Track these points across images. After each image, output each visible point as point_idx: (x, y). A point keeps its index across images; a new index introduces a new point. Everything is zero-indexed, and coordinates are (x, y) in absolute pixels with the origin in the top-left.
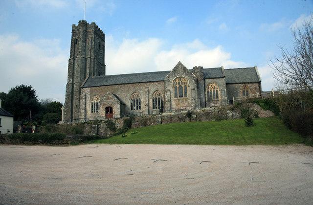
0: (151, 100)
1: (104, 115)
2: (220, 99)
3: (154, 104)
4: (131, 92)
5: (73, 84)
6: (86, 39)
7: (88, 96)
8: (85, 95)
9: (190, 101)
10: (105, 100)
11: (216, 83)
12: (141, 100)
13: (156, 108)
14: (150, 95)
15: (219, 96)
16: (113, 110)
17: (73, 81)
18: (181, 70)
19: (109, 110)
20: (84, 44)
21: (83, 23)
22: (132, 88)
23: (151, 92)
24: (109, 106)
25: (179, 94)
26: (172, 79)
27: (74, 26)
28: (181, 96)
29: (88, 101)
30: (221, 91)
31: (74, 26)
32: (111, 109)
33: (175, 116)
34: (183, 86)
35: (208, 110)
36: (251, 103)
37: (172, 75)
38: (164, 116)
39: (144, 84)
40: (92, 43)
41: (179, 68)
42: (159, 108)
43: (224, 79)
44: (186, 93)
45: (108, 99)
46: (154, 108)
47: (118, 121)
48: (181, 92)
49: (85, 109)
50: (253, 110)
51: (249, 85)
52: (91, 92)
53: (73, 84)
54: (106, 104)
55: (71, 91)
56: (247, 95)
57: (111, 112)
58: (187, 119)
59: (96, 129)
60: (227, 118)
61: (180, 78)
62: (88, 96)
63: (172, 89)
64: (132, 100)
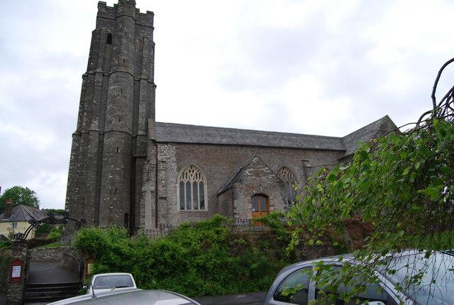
24: (261, 191)
45: (258, 175)
54: (253, 188)
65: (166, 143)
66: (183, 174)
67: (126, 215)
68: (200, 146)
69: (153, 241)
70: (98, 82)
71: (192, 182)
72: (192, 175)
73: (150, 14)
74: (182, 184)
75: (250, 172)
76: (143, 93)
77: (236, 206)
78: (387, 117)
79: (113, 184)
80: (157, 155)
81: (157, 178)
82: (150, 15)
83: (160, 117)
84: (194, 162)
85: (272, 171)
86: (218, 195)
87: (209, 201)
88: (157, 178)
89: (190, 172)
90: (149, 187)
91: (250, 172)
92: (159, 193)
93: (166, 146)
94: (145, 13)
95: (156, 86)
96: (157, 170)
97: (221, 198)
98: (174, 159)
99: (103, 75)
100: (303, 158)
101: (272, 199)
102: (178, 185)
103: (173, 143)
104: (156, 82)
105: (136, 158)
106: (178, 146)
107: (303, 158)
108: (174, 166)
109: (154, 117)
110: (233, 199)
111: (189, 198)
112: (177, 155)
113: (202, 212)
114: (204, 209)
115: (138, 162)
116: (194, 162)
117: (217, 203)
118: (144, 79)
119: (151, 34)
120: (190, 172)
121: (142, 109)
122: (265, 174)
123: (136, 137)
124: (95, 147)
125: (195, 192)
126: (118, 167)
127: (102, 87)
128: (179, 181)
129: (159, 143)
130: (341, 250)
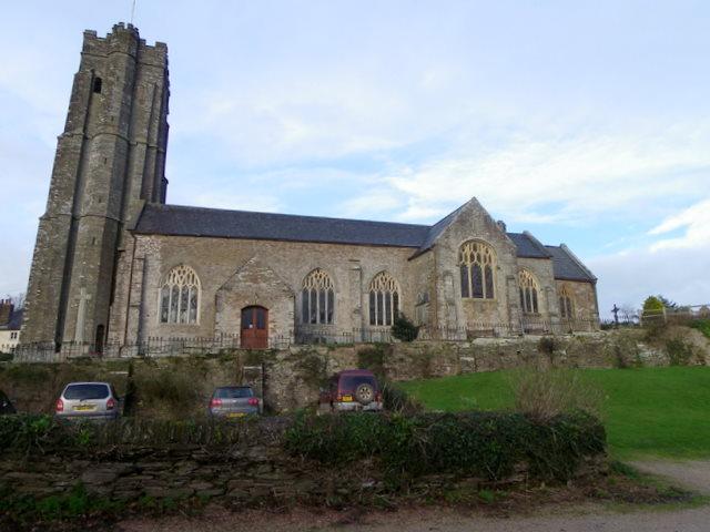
0: (367, 298)
1: (237, 332)
2: (541, 310)
3: (372, 310)
4: (307, 269)
5: (74, 219)
6: (134, 85)
7: (155, 264)
8: (145, 260)
9: (503, 311)
10: (242, 284)
11: (533, 270)
12: (337, 297)
13: (380, 323)
14: (364, 282)
15: (540, 303)
16: (270, 318)
17: (74, 209)
18: (478, 224)
19: (254, 316)
20: (129, 98)
21: (128, 36)
22: (309, 255)
23: (368, 276)
24: (258, 302)
25: (473, 286)
26: (456, 244)
27: (90, 36)
28: (478, 294)
29: (153, 281)
30: (546, 290)
31: (90, 36)
32: (262, 310)
33: (508, 348)
34: (483, 266)
35: (591, 337)
36: (686, 328)
37: (456, 231)
38: (480, 348)
39: (347, 248)
40: (154, 101)
41: (470, 217)
42: (388, 323)
43: (549, 262)
44: (490, 286)
45: (255, 280)
46: (372, 322)
47: (337, 353)
48: (477, 282)
49: (141, 308)
50: (691, 346)
51: (573, 284)
52: (166, 253)
53: (74, 219)
54: (246, 297)
55: (66, 240)
56: (570, 316)
57: (262, 325)
58: (544, 360)
59: (258, 383)
60: (640, 363)
61: (475, 244)
62: (155, 264)
63: (456, 271)
64: (166, 287)
71: (180, 286)
73: (162, 47)
75: (243, 277)
77: (217, 320)
78: (474, 199)
82: (162, 47)
85: (276, 274)
87: (202, 313)
89: (179, 272)
90: (117, 290)
91: (243, 277)
92: (132, 301)
94: (154, 45)
95: (41, 219)
100: (350, 256)
107: (350, 256)
112: (163, 250)
122: (266, 280)
126: (93, 264)
130: (29, 472)
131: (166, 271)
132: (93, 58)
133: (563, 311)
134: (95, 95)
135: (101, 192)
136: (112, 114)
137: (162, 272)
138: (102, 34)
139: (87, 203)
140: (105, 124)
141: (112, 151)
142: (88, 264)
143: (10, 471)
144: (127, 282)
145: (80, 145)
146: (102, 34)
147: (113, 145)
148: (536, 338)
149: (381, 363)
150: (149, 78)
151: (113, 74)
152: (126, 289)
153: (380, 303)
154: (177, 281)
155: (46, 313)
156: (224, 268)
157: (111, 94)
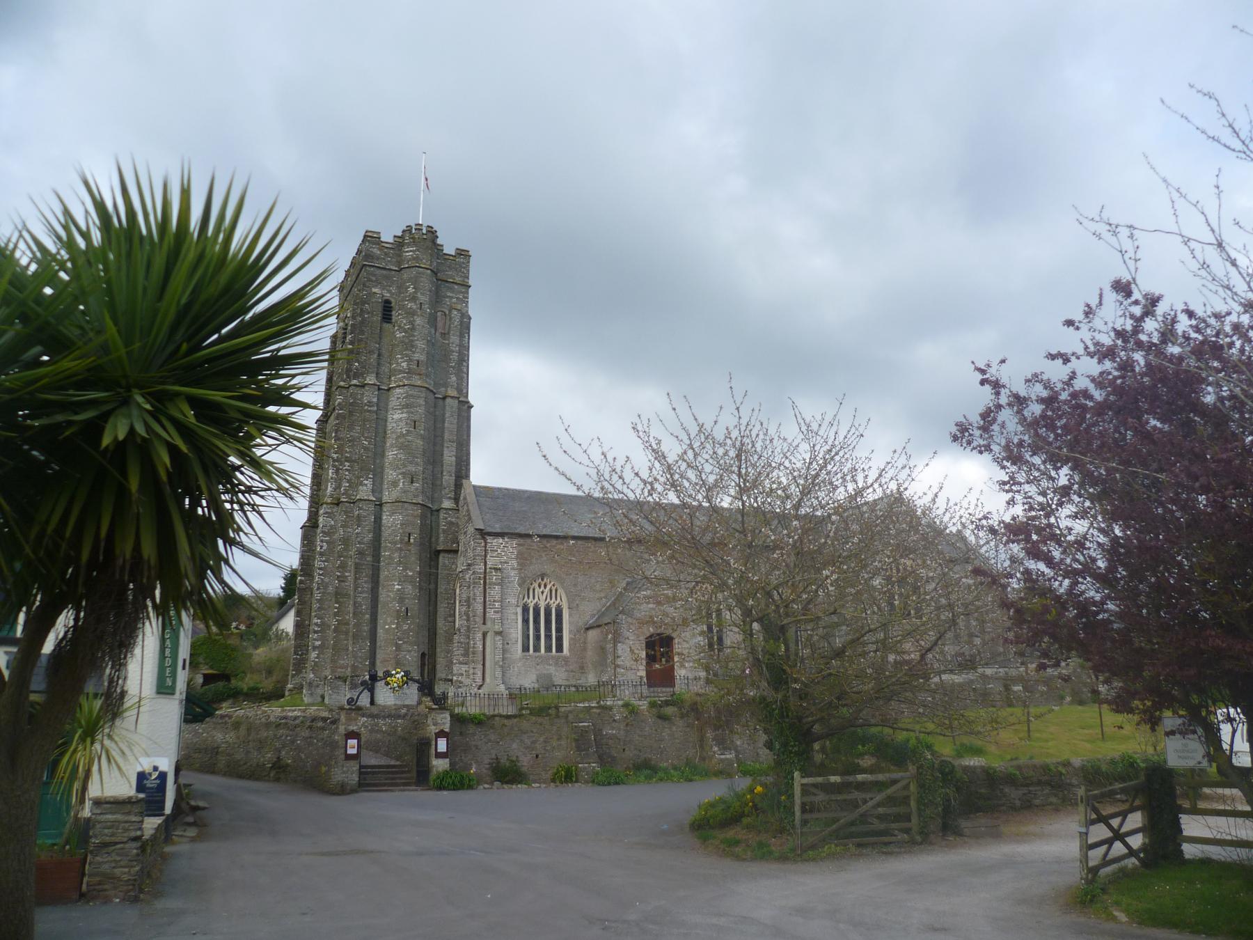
31: (370, 238)
65: (501, 535)
66: (551, 591)
67: (423, 655)
68: (560, 541)
69: (440, 769)
70: (370, 404)
72: (543, 592)
73: (463, 254)
74: (525, 609)
76: (450, 423)
77: (620, 652)
79: (401, 600)
80: (486, 556)
81: (485, 597)
82: (463, 254)
83: (482, 473)
84: (548, 568)
86: (587, 629)
87: (571, 639)
88: (485, 597)
89: (540, 586)
93: (501, 541)
96: (485, 583)
97: (592, 634)
98: (515, 563)
99: (379, 389)
101: (679, 643)
102: (519, 610)
103: (512, 534)
104: (471, 399)
105: (439, 552)
106: (522, 541)
108: (514, 576)
109: (467, 476)
110: (616, 641)
111: (537, 638)
112: (520, 556)
113: (559, 657)
114: (562, 651)
115: (443, 559)
116: (548, 568)
117: (585, 643)
118: (452, 397)
119: (465, 300)
120: (540, 586)
121: (449, 457)
123: (438, 511)
124: (369, 531)
125: (548, 628)
126: (410, 571)
127: (376, 412)
128: (521, 604)
129: (490, 534)
131: (526, 586)
132: (378, 272)
133: (711, 645)
134: (386, 326)
135: (412, 468)
136: (416, 356)
137: (520, 585)
138: (387, 237)
139: (395, 484)
140: (410, 372)
141: (421, 410)
142: (405, 569)
143: (1014, 724)
144: (480, 599)
145: (375, 400)
146: (387, 237)
147: (422, 402)
148: (620, 703)
149: (501, 740)
150: (451, 297)
151: (413, 298)
152: (480, 608)
153: (548, 622)
154: (540, 598)
155: (355, 637)
156: (593, 581)
157: (413, 329)
